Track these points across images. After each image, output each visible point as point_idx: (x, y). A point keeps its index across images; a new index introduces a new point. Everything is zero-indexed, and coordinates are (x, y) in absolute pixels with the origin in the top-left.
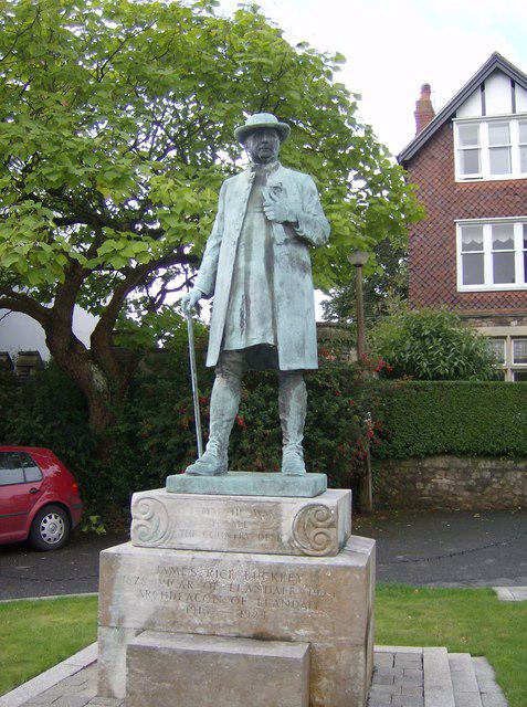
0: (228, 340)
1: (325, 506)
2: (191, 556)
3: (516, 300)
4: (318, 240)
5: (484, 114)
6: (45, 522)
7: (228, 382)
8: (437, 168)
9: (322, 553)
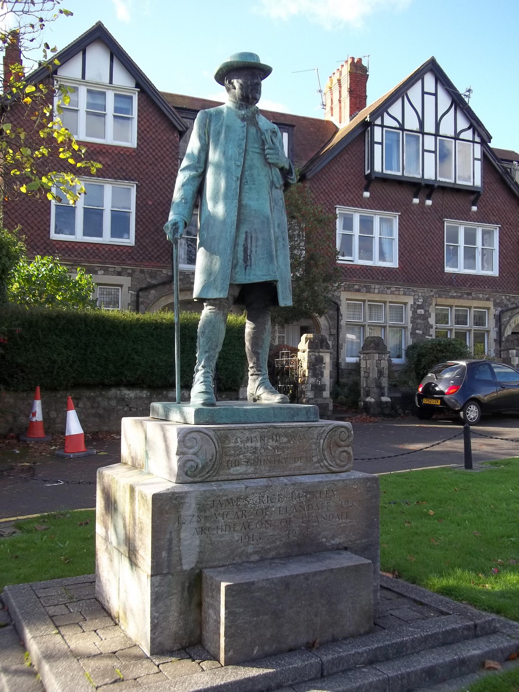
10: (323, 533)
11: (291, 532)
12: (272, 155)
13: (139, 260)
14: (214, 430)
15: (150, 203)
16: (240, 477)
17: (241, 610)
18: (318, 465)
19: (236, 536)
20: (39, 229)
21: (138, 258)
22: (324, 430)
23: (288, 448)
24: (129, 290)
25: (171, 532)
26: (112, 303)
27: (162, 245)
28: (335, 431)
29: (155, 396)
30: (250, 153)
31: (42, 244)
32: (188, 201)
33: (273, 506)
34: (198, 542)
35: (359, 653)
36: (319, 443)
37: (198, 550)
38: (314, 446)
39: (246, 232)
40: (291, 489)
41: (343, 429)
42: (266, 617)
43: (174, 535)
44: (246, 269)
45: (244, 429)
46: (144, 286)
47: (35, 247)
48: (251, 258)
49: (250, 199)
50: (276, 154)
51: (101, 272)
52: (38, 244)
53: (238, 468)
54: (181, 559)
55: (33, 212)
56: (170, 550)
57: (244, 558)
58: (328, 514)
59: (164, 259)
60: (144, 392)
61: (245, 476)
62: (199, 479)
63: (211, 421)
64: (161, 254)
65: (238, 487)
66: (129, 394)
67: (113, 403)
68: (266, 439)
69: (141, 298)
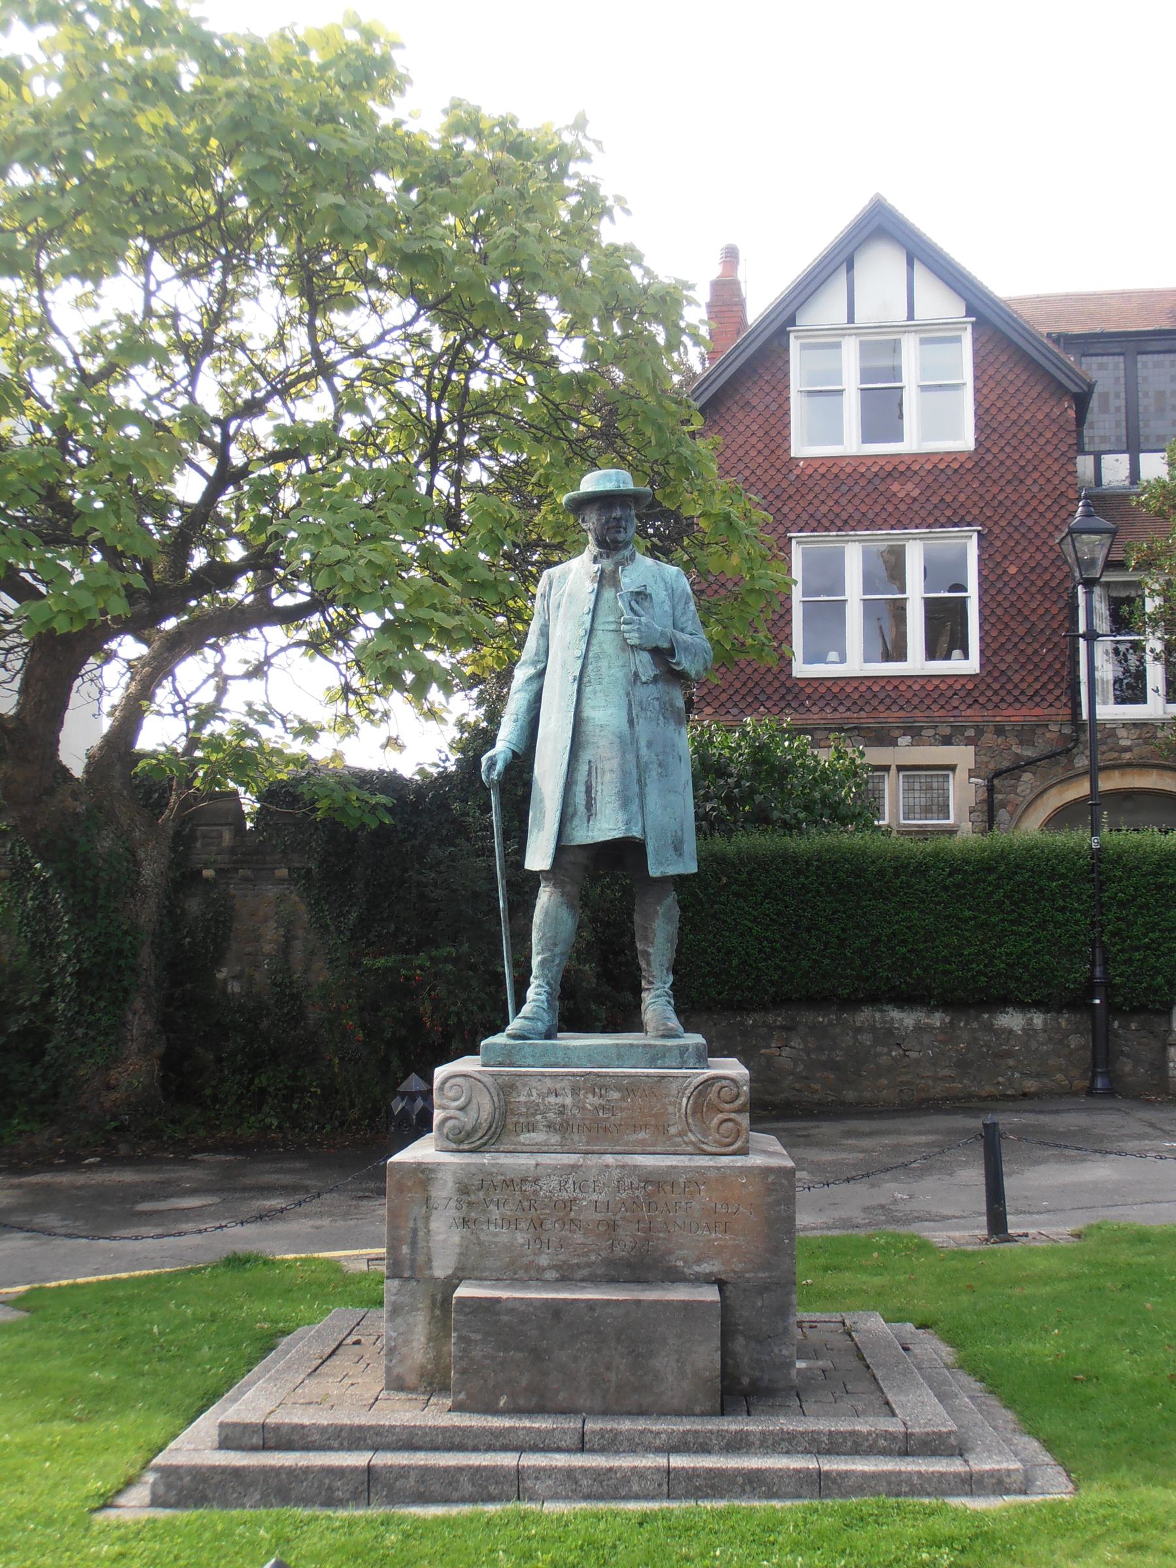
0: (568, 830)
1: (733, 1080)
2: (534, 1162)
3: (909, 695)
4: (697, 673)
5: (851, 319)
7: (563, 894)
8: (754, 427)
9: (731, 1148)
10: (677, 1252)
11: (616, 1243)
13: (990, 705)
14: (492, 1075)
15: (1013, 570)
16: (535, 1148)
17: (479, 1337)
18: (679, 1139)
19: (520, 1238)
21: (989, 700)
22: (690, 1083)
23: (622, 1109)
24: (970, 777)
25: (415, 1220)
26: (935, 808)
27: (1044, 666)
28: (712, 1084)
29: (962, 1024)
30: (599, 633)
33: (584, 1199)
34: (456, 1239)
35: (652, 1432)
36: (680, 1104)
37: (458, 1251)
38: (671, 1109)
40: (616, 1174)
41: (724, 1083)
42: (519, 1355)
43: (420, 1224)
45: (543, 1075)
46: (1006, 764)
49: (593, 708)
51: (904, 740)
53: (533, 1135)
54: (430, 1260)
56: (413, 1244)
57: (533, 1273)
58: (688, 1221)
59: (1050, 698)
60: (937, 1015)
61: (545, 1148)
62: (466, 1147)
64: (1043, 686)
65: (525, 1161)
66: (901, 1020)
67: (866, 1039)
69: (1000, 792)
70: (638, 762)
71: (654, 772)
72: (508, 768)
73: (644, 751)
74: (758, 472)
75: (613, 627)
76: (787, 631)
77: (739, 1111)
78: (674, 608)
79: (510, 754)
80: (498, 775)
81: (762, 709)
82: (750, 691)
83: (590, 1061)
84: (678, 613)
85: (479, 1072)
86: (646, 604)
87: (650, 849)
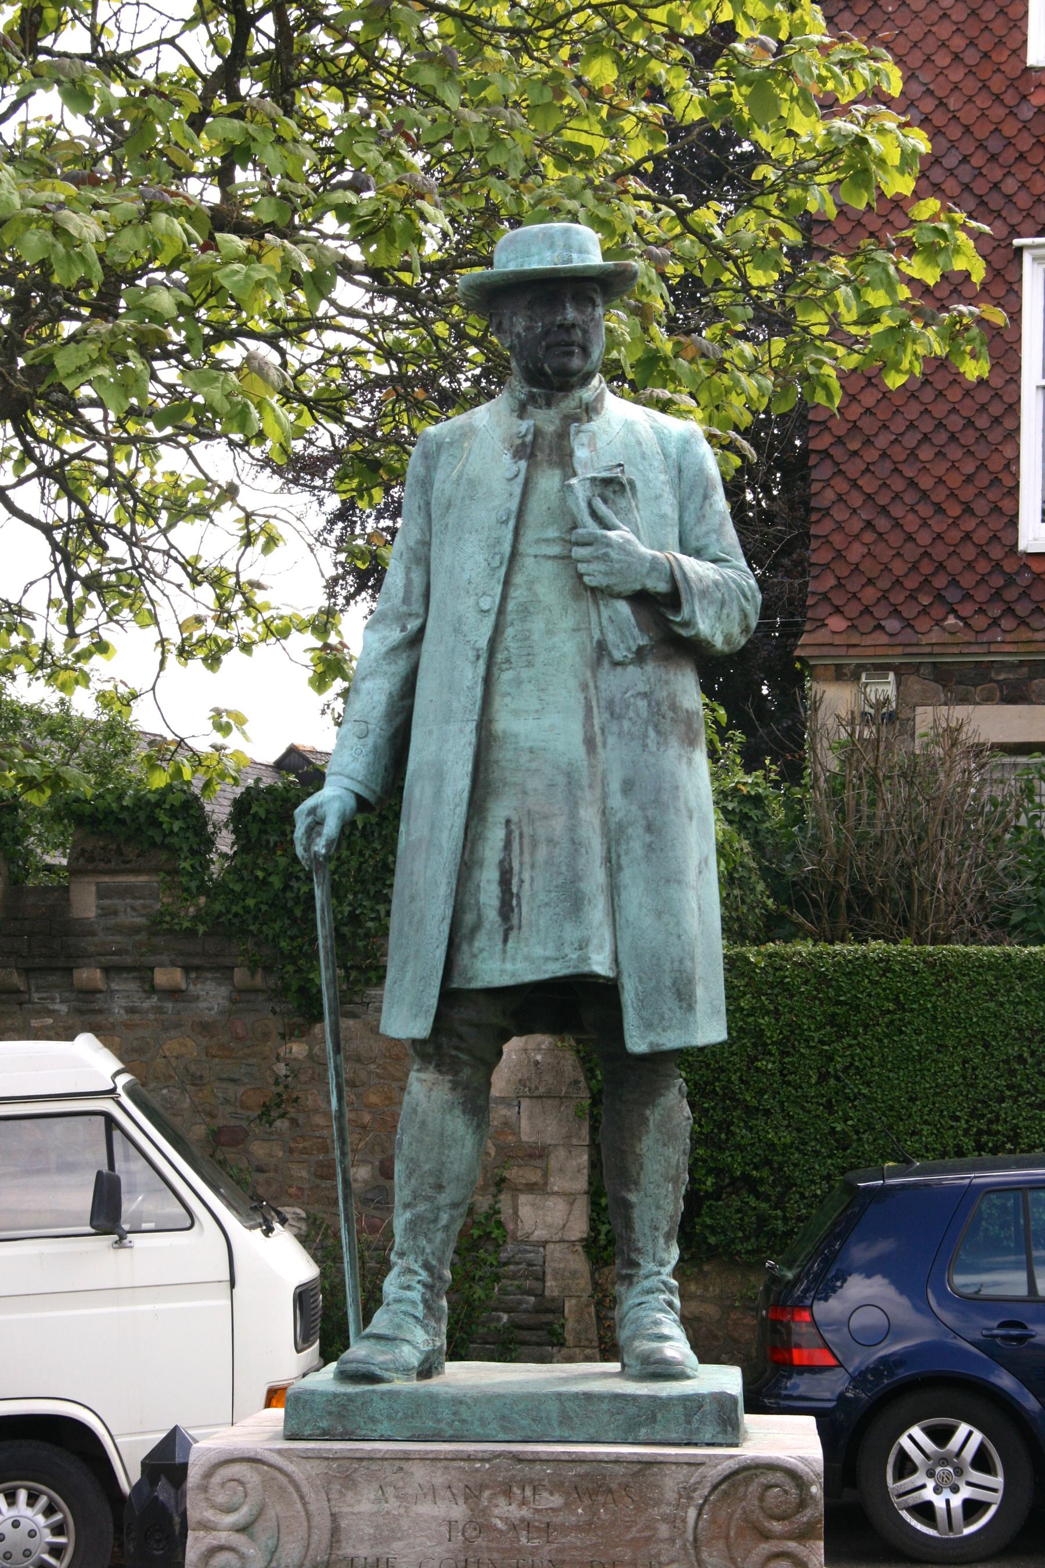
0: (463, 958)
6: (58, 1530)
7: (455, 1086)
12: (588, 562)
20: (968, 509)
28: (747, 1482)
30: (529, 562)
31: (983, 580)
32: (371, 727)
36: (684, 1521)
38: (664, 1530)
39: (508, 822)
44: (505, 940)
45: (406, 1457)
47: (952, 595)
48: (519, 904)
49: (516, 713)
50: (597, 558)
52: (967, 580)
55: (941, 437)
63: (340, 1429)
68: (487, 1493)
70: (605, 822)
71: (636, 844)
72: (348, 826)
73: (617, 801)
74: (953, 103)
75: (556, 550)
76: (1009, 453)
77: (803, 1535)
78: (682, 508)
79: (352, 802)
80: (328, 846)
81: (951, 620)
82: (927, 581)
83: (504, 1429)
84: (690, 518)
85: (280, 1452)
86: (623, 503)
87: (629, 996)
